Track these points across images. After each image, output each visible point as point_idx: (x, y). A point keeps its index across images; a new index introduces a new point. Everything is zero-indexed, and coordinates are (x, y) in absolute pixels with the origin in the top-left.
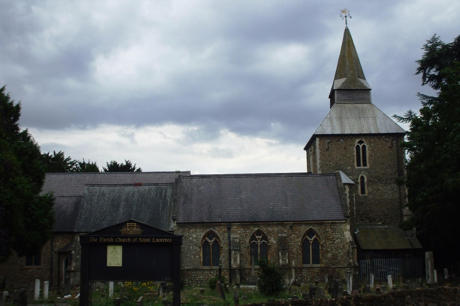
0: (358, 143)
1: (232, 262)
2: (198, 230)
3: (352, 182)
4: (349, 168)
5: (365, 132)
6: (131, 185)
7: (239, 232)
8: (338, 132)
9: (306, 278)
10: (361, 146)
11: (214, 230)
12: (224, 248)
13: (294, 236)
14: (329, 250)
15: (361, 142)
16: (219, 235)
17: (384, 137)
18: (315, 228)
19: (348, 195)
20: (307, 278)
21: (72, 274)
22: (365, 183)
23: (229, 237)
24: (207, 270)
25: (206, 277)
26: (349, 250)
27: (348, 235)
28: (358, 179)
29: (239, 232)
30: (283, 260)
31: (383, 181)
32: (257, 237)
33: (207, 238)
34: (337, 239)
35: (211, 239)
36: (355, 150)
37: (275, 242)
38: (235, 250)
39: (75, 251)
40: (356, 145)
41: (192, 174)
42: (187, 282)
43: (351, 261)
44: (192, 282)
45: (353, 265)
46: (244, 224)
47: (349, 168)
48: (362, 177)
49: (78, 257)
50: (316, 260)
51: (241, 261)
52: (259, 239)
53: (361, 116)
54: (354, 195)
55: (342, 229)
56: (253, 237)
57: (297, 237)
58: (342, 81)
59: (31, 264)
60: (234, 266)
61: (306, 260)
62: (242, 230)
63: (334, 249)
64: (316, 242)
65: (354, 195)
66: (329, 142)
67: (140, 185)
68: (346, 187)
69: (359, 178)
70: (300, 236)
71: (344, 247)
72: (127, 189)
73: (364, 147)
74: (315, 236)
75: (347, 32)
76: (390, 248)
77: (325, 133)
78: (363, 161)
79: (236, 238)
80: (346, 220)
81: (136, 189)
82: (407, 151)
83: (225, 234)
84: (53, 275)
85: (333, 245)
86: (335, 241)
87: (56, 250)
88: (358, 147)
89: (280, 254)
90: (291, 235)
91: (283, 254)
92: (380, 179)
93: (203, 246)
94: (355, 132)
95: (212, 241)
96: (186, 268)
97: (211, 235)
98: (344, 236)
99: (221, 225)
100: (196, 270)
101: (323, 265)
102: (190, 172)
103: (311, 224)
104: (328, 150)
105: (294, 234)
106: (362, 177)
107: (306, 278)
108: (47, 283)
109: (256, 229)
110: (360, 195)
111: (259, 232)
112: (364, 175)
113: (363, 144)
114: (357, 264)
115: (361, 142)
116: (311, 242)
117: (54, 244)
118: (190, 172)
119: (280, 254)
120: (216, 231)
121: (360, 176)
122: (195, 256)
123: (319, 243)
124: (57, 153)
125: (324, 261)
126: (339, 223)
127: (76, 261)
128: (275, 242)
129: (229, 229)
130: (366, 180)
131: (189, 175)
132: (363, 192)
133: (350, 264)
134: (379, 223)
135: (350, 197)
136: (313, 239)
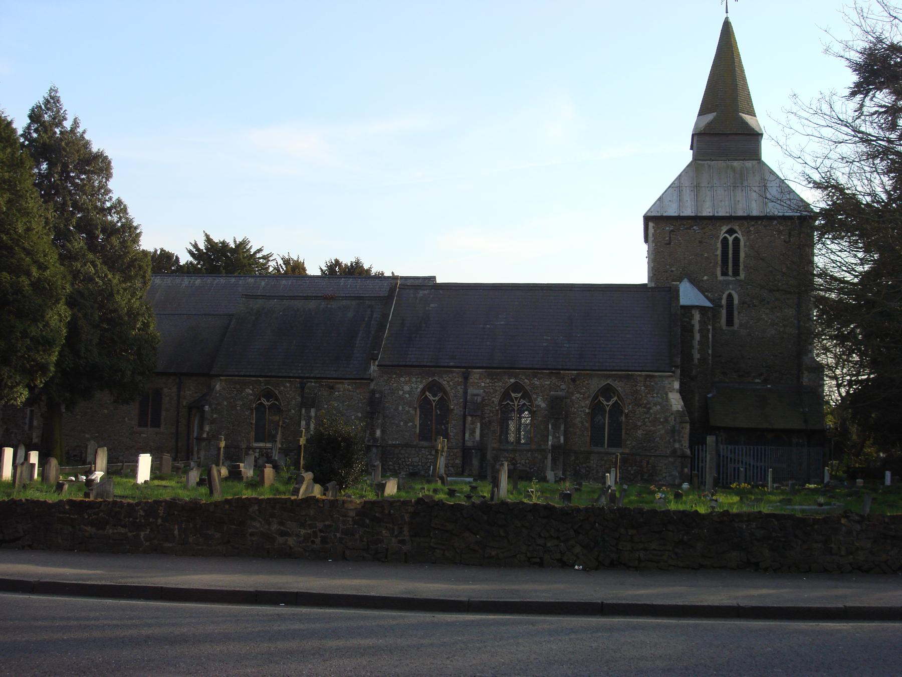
0: (726, 232)
1: (467, 435)
2: (414, 379)
3: (708, 304)
4: (705, 278)
5: (740, 213)
6: (316, 298)
7: (483, 384)
8: (688, 212)
9: (594, 472)
10: (731, 239)
11: (441, 381)
12: (455, 412)
13: (578, 395)
14: (639, 424)
15: (731, 232)
16: (448, 389)
17: (775, 222)
18: (618, 385)
19: (697, 327)
20: (597, 472)
21: (204, 444)
22: (735, 307)
23: (465, 393)
24: (425, 448)
25: (424, 460)
26: (674, 427)
27: (676, 401)
28: (721, 299)
29: (483, 384)
30: (554, 437)
31: (768, 303)
32: (513, 395)
33: (427, 393)
34: (655, 405)
35: (434, 396)
36: (719, 245)
37: (543, 405)
38: (472, 416)
39: (210, 406)
40: (721, 238)
41: (438, 281)
42: (391, 467)
43: (677, 445)
44: (399, 468)
45: (679, 453)
46: (492, 370)
47: (705, 278)
48: (730, 296)
49: (215, 416)
50: (616, 441)
51: (481, 435)
52: (516, 398)
53: (739, 181)
54: (710, 327)
55: (664, 387)
56: (506, 395)
57: (584, 398)
58: (710, 117)
59: (146, 426)
60: (469, 444)
61: (597, 439)
62: (488, 381)
63: (648, 424)
64: (617, 409)
65: (710, 327)
66: (672, 231)
67: (332, 298)
68: (693, 312)
69: (725, 296)
70: (589, 397)
71: (666, 420)
72: (312, 305)
73: (736, 240)
74: (615, 398)
75: (727, 30)
76: (765, 426)
77: (665, 214)
78: (733, 266)
79: (477, 395)
80: (673, 372)
81: (323, 304)
82: (109, 217)
83: (459, 388)
84: (179, 444)
85: (647, 416)
86: (650, 408)
87: (184, 403)
88: (725, 240)
89: (550, 426)
90: (573, 394)
91: (556, 427)
92: (764, 300)
93: (420, 406)
94: (722, 213)
95: (437, 398)
96: (390, 442)
97: (434, 387)
98: (667, 400)
99: (452, 372)
100: (407, 446)
101: (627, 451)
102: (434, 278)
103: (609, 376)
104: (669, 244)
105: (578, 392)
106: (730, 297)
107: (594, 472)
108: (512, 438)
109: (512, 381)
110: (724, 327)
111: (517, 387)
112: (733, 293)
113: (734, 236)
114: (688, 452)
115: (731, 232)
116: (608, 409)
117: (182, 393)
118: (434, 278)
119: (550, 426)
120: (445, 381)
121: (727, 293)
122: (406, 423)
123: (622, 412)
124: (239, 240)
125: (628, 442)
126: (660, 376)
127: (212, 423)
128: (543, 405)
129: (466, 378)
130: (736, 301)
131: (431, 283)
132: (730, 321)
133: (674, 451)
134: (757, 381)
135: (700, 331)
136: (611, 403)
